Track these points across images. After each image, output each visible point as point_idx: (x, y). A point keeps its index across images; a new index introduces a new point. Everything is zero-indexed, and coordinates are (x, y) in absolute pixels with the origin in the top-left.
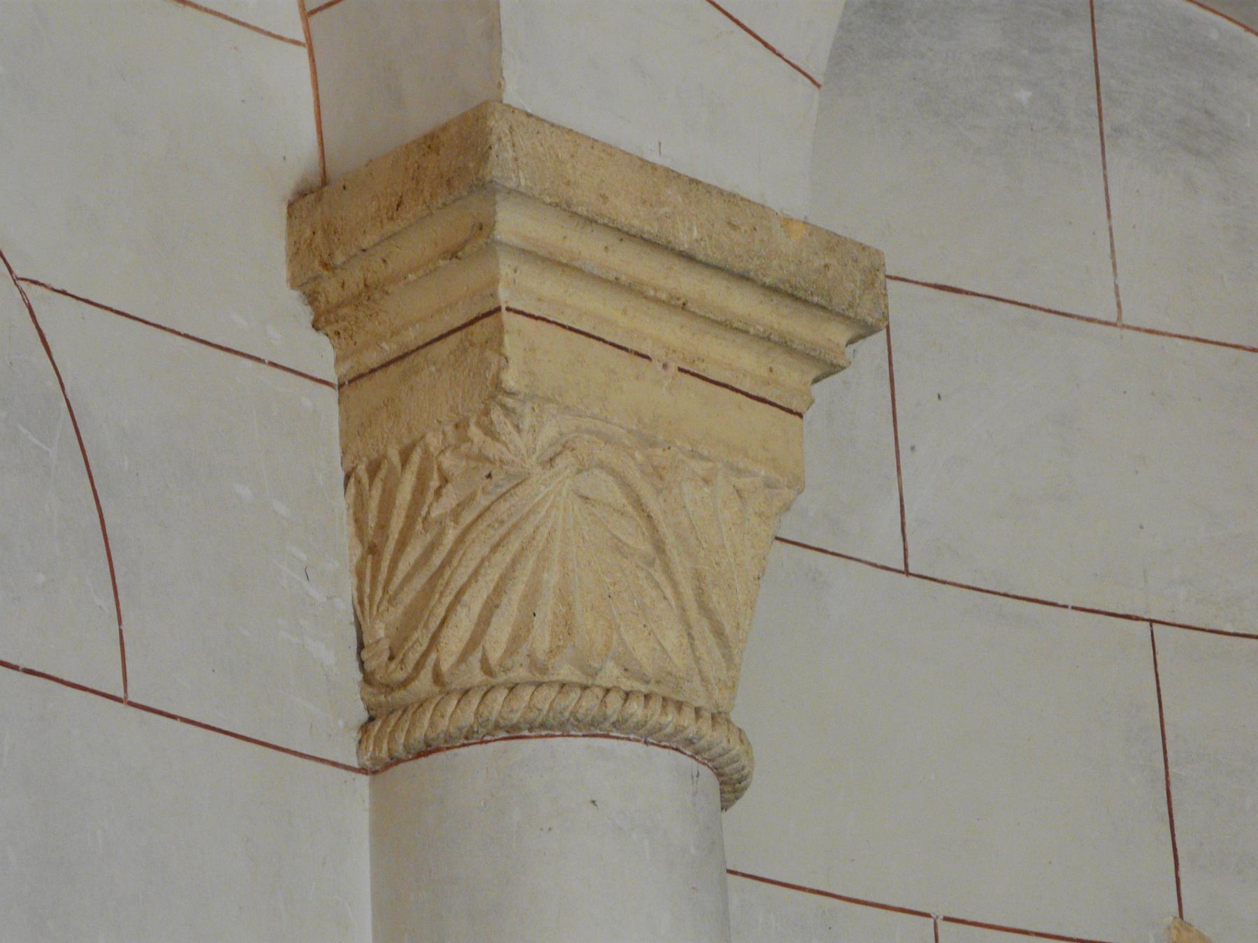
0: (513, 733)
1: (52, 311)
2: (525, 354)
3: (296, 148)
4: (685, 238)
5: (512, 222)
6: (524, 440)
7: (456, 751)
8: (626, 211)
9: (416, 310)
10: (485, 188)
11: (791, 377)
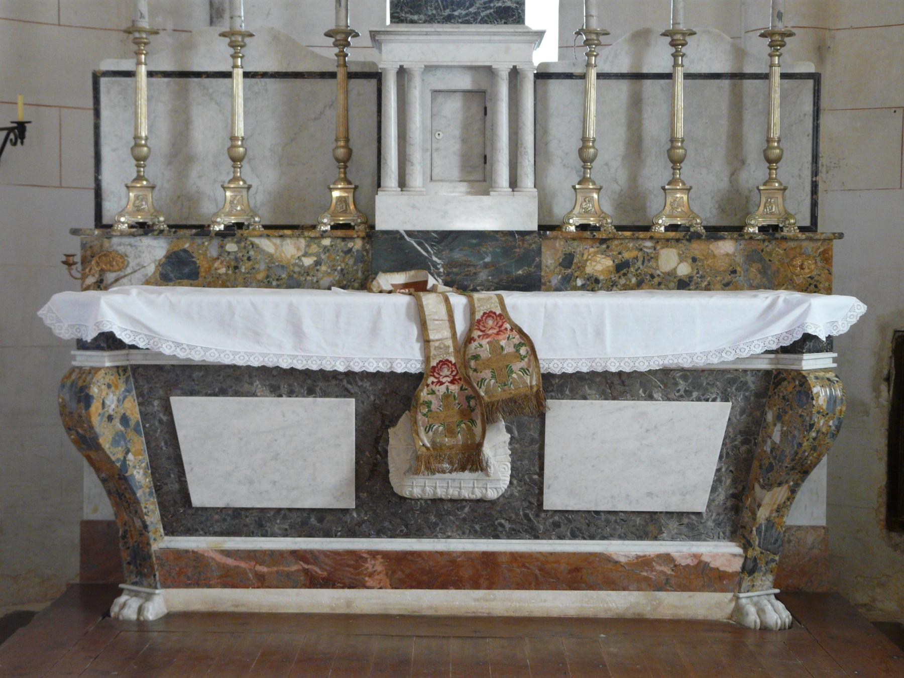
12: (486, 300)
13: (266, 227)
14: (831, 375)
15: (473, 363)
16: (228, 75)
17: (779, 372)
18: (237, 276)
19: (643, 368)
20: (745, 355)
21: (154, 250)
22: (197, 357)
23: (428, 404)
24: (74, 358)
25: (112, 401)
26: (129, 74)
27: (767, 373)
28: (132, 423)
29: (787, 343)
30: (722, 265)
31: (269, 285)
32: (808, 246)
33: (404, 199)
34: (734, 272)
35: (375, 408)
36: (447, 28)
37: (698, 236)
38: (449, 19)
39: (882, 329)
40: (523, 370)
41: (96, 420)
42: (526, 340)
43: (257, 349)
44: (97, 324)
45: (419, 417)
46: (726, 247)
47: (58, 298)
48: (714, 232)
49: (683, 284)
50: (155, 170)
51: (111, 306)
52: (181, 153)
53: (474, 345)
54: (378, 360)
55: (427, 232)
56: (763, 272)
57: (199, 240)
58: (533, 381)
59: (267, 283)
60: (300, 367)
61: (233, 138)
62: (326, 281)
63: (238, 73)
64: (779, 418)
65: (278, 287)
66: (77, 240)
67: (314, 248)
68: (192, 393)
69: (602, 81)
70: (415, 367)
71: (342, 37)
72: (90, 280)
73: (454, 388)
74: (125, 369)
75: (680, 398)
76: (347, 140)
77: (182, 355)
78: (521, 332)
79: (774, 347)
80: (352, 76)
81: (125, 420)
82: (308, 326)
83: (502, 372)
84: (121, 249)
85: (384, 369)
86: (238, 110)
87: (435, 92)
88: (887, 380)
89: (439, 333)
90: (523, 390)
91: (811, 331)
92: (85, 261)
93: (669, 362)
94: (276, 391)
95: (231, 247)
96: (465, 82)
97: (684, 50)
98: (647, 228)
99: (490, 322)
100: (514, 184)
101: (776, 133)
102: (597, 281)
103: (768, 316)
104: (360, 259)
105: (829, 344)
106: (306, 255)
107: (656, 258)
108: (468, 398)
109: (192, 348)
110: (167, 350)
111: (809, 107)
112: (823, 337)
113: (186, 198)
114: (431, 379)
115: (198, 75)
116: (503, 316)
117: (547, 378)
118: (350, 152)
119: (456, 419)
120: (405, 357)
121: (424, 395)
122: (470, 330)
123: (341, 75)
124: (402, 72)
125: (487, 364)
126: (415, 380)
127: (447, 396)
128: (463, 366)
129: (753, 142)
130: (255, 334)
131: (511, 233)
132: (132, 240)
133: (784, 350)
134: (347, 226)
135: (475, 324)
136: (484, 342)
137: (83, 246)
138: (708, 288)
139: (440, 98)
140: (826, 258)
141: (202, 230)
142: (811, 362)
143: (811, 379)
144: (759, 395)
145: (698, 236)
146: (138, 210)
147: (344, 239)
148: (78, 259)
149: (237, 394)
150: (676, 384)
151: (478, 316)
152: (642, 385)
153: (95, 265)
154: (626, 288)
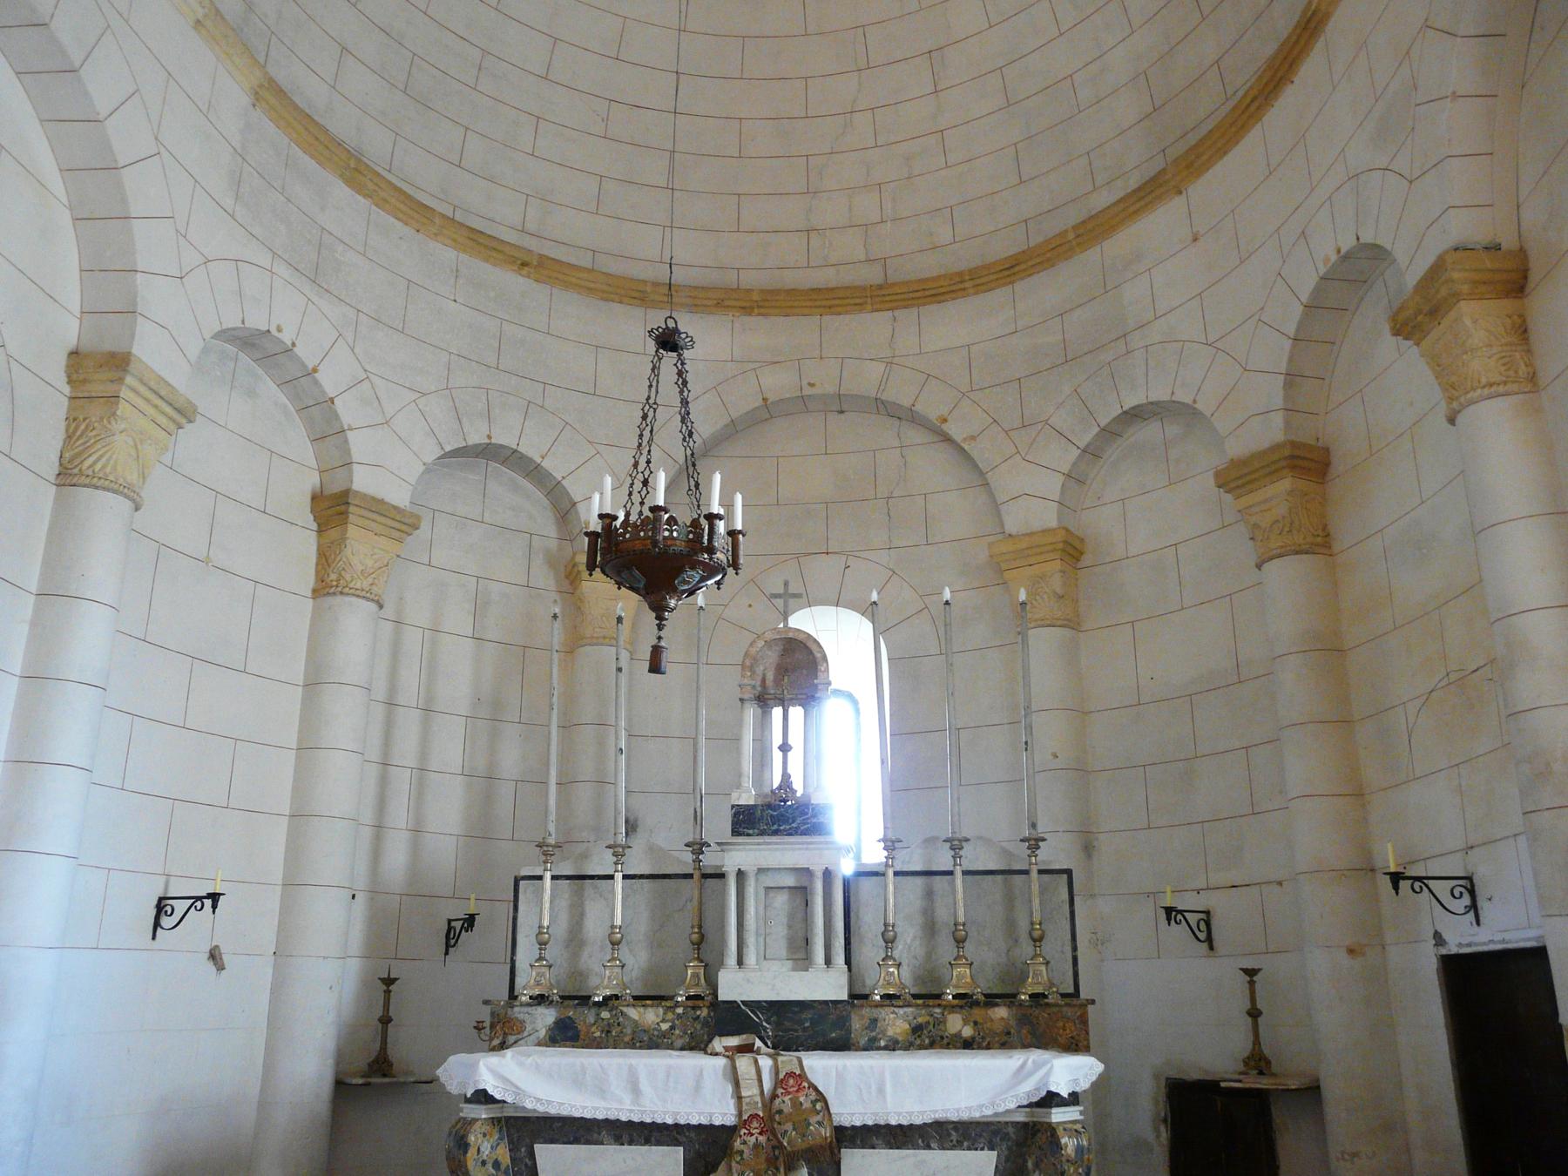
0: (97, 488)
1: (13, 364)
2: (123, 409)
3: (72, 342)
4: (163, 393)
5: (129, 380)
6: (117, 426)
7: (354, 599)
8: (152, 384)
9: (96, 389)
10: (125, 370)
11: (172, 427)
12: (788, 1060)
13: (636, 998)
14: (1078, 1127)
15: (777, 1117)
16: (611, 877)
17: (1035, 1124)
18: (610, 1038)
19: (918, 1121)
20: (1001, 1110)
21: (545, 1018)
22: (553, 1111)
23: (741, 1153)
24: (461, 1110)
25: (486, 1148)
26: (540, 878)
27: (1025, 1124)
28: (503, 1167)
29: (1035, 1099)
30: (998, 1027)
31: (633, 1047)
32: (1068, 1012)
33: (740, 975)
34: (1009, 1033)
35: (699, 1155)
36: (774, 839)
37: (977, 1003)
38: (776, 833)
39: (1156, 1077)
40: (819, 1123)
41: (470, 1164)
42: (821, 1098)
43: (602, 1104)
44: (476, 1082)
45: (733, 1164)
46: (1001, 1012)
47: (452, 1059)
48: (991, 999)
49: (968, 1044)
50: (554, 952)
51: (492, 1071)
52: (575, 940)
53: (778, 1101)
54: (700, 1114)
55: (759, 1002)
56: (1033, 1033)
57: (580, 1009)
58: (826, 1132)
59: (632, 1045)
60: (636, 1120)
61: (613, 927)
62: (679, 1043)
63: (619, 876)
64: (1037, 1165)
65: (641, 1048)
66: (488, 1009)
67: (670, 1016)
68: (552, 1142)
69: (899, 878)
70: (730, 1120)
71: (698, 847)
72: (496, 1042)
73: (761, 1138)
74: (499, 1120)
75: (953, 1148)
76: (700, 927)
77: (541, 1109)
78: (816, 1089)
79: (1025, 1103)
80: (705, 876)
81: (496, 1164)
82: (644, 1085)
83: (802, 1126)
84: (521, 1016)
85: (704, 1121)
86: (617, 905)
87: (768, 889)
88: (1165, 1121)
89: (750, 1091)
90: (819, 1141)
91: (1053, 1089)
92: (492, 1026)
93: (939, 1116)
94: (619, 1141)
95: (605, 1014)
96: (790, 881)
97: (962, 853)
98: (938, 996)
99: (791, 1081)
100: (828, 962)
101: (1037, 918)
102: (897, 1042)
103: (1020, 1074)
104: (705, 1024)
105: (1074, 1099)
106: (663, 1021)
107: (945, 1022)
108: (774, 1148)
109: (549, 1102)
110: (529, 1106)
111: (1065, 896)
112: (1065, 1094)
113: (578, 975)
114: (744, 1131)
115: (592, 877)
116: (802, 1077)
117: (840, 1131)
118: (702, 937)
119: (764, 1166)
120: (721, 1111)
121: (737, 1144)
122: (775, 1088)
123: (697, 875)
124: (741, 874)
125: (789, 1118)
126: (729, 1132)
127: (757, 1145)
128: (769, 1119)
129: (1023, 925)
130: (601, 1091)
131: (826, 1002)
132: (529, 1009)
133: (1030, 1105)
134: (697, 997)
135: (779, 1083)
136: (786, 1099)
137: (493, 1014)
138: (988, 1047)
139: (772, 894)
140: (1083, 1020)
141: (584, 1000)
142: (1058, 1115)
143: (1060, 1131)
144: (1019, 1144)
145: (977, 1003)
146: (538, 984)
147: (694, 1008)
148: (487, 1024)
149: (588, 1142)
150: (949, 1135)
151: (781, 1076)
152: (921, 1136)
153: (499, 1031)
154: (922, 1047)
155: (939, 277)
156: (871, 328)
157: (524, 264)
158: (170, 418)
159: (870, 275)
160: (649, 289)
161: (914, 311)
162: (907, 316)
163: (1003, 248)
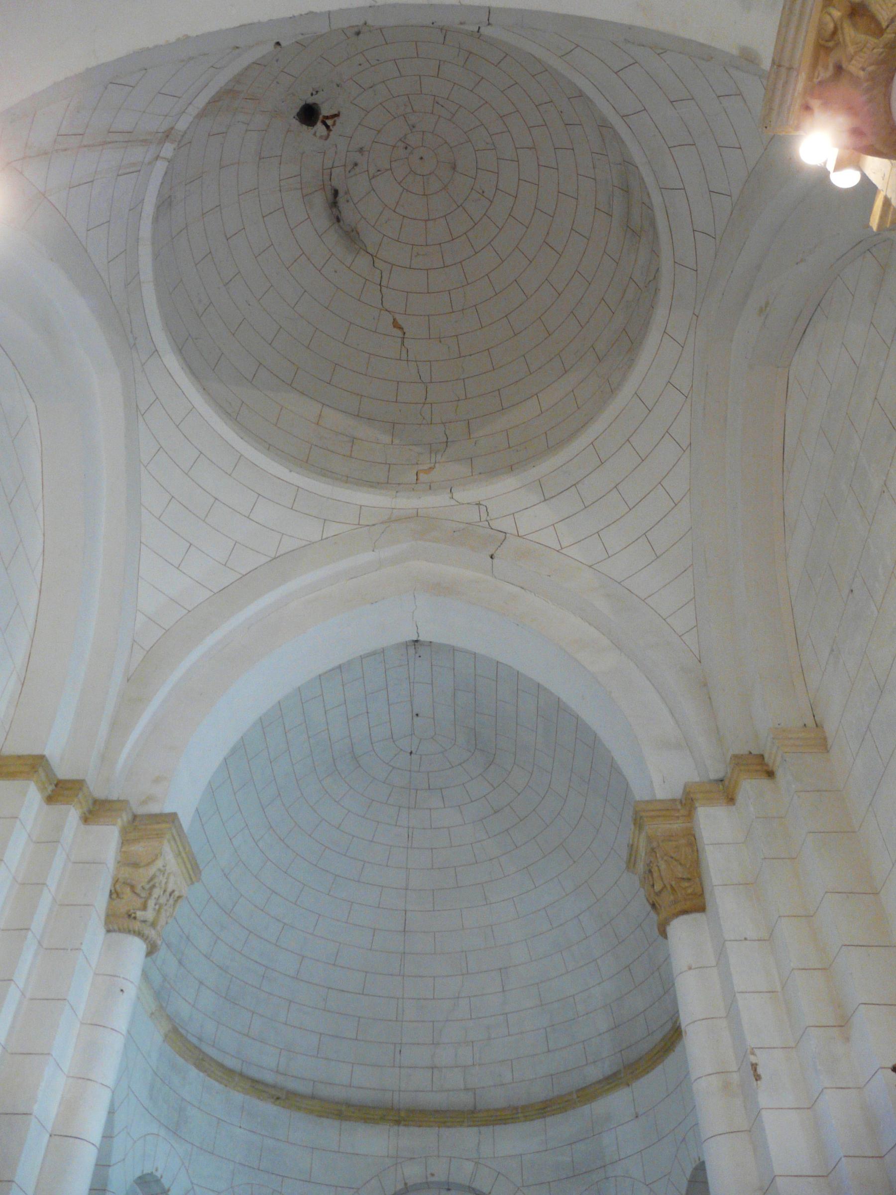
148: (779, 989)
155: (504, 1109)
156: (466, 1137)
157: (278, 1098)
158: (798, 30)
159: (464, 1100)
160: (344, 1108)
161: (491, 1127)
162: (487, 1131)
163: (540, 1092)
